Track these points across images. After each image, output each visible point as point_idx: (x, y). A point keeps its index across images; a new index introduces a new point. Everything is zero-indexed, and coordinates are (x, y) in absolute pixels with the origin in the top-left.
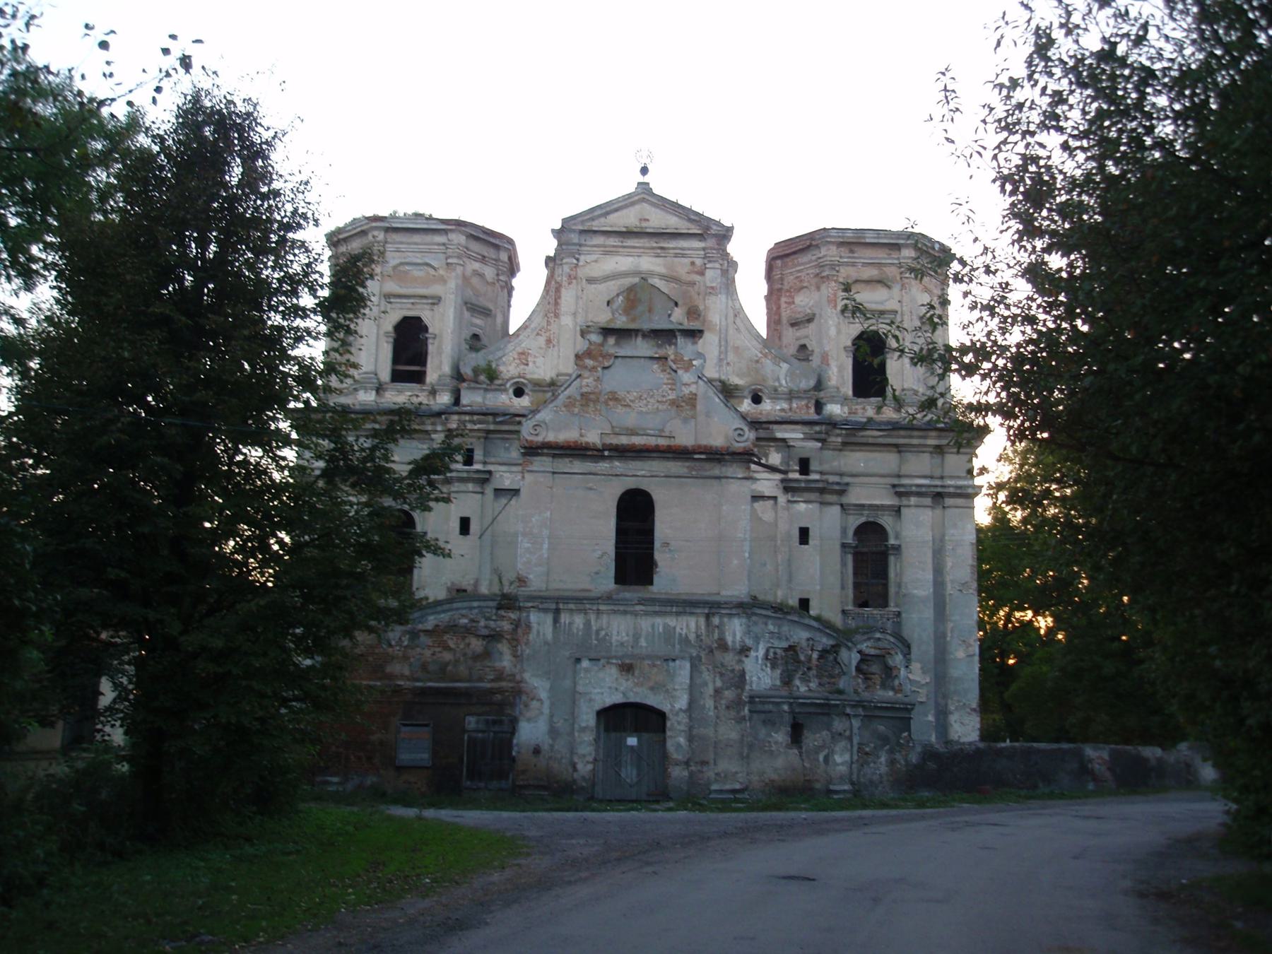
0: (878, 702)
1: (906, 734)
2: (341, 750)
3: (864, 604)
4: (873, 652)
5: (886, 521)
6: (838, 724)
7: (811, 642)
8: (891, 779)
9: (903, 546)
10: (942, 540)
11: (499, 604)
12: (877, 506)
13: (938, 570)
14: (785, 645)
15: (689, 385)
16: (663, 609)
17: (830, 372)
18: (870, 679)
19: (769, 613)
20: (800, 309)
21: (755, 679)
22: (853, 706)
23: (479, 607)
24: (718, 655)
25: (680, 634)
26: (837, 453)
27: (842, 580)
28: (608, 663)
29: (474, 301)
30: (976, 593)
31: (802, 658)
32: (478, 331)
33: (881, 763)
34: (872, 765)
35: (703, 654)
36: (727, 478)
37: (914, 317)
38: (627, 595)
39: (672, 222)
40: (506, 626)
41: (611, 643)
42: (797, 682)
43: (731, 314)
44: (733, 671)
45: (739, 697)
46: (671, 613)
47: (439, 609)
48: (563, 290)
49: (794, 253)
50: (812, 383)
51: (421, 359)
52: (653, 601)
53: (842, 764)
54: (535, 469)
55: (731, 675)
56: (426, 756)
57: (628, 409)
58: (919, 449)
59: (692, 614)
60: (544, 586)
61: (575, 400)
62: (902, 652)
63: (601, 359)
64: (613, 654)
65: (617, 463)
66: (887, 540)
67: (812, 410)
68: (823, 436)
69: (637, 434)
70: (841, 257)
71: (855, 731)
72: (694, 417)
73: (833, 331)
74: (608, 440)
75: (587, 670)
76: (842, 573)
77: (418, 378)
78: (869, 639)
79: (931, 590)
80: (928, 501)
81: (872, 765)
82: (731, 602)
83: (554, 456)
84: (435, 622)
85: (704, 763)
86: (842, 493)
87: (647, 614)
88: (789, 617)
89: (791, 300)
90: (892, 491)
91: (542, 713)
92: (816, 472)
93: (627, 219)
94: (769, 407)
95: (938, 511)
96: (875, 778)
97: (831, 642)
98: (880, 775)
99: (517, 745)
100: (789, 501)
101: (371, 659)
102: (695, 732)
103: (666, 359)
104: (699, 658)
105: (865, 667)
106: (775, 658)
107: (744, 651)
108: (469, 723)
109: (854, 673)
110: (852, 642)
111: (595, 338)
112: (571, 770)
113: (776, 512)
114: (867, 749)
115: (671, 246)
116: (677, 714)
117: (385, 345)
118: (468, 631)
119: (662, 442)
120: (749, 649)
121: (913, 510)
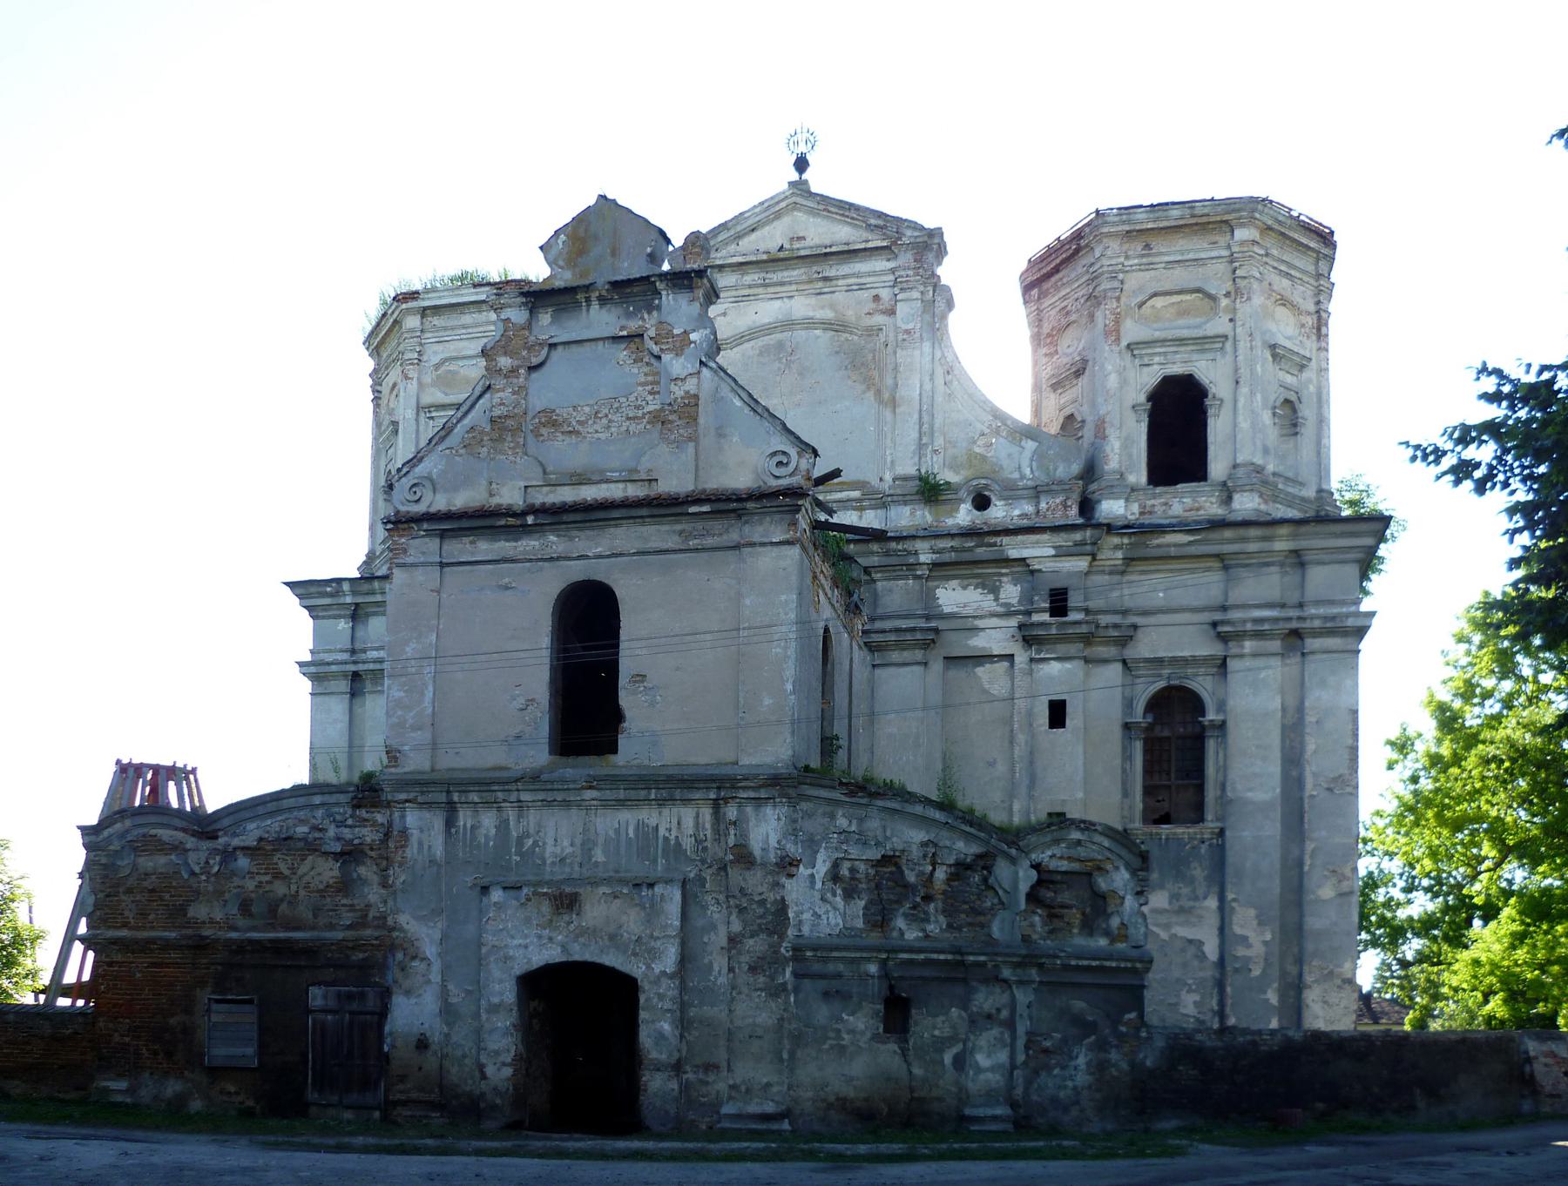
0: (1070, 956)
1: (1133, 1015)
2: (127, 1039)
3: (1165, 819)
4: (1064, 866)
5: (1203, 685)
6: (986, 999)
8: (1098, 1096)
9: (1230, 724)
10: (1300, 709)
14: (875, 854)
15: (683, 380)
16: (632, 794)
17: (1108, 449)
18: (1060, 917)
21: (806, 916)
22: (1016, 965)
23: (323, 804)
24: (736, 876)
25: (666, 839)
27: (1124, 783)
31: (911, 877)
34: (1056, 1071)
35: (707, 874)
36: (752, 545)
37: (1258, 343)
38: (569, 772)
39: (842, 234)
40: (369, 835)
42: (900, 923)
43: (939, 371)
44: (762, 903)
45: (775, 949)
50: (1076, 468)
52: (614, 781)
53: (992, 1069)
54: (409, 560)
55: (760, 911)
56: (250, 1051)
58: (1262, 562)
59: (686, 801)
60: (427, 766)
61: (482, 432)
62: (1128, 866)
63: (524, 353)
64: (547, 877)
66: (1203, 713)
70: (1127, 257)
71: (1021, 1008)
72: (693, 438)
73: (1113, 381)
76: (1124, 771)
78: (1057, 842)
79: (1278, 790)
80: (1275, 645)
82: (756, 776)
83: (443, 535)
84: (257, 833)
85: (710, 1067)
86: (1124, 641)
87: (605, 804)
90: (1212, 633)
91: (429, 982)
92: (1078, 609)
93: (771, 238)
94: (998, 512)
97: (974, 849)
98: (1075, 1088)
99: (391, 1034)
100: (1032, 660)
101: (167, 896)
102: (692, 1012)
103: (642, 335)
104: (701, 881)
105: (1050, 894)
106: (852, 879)
107: (787, 865)
109: (1023, 906)
110: (1019, 849)
111: (518, 315)
113: (1012, 679)
114: (1048, 1044)
115: (841, 273)
116: (657, 982)
118: (311, 847)
119: (634, 491)
120: (795, 863)
121: (1248, 663)
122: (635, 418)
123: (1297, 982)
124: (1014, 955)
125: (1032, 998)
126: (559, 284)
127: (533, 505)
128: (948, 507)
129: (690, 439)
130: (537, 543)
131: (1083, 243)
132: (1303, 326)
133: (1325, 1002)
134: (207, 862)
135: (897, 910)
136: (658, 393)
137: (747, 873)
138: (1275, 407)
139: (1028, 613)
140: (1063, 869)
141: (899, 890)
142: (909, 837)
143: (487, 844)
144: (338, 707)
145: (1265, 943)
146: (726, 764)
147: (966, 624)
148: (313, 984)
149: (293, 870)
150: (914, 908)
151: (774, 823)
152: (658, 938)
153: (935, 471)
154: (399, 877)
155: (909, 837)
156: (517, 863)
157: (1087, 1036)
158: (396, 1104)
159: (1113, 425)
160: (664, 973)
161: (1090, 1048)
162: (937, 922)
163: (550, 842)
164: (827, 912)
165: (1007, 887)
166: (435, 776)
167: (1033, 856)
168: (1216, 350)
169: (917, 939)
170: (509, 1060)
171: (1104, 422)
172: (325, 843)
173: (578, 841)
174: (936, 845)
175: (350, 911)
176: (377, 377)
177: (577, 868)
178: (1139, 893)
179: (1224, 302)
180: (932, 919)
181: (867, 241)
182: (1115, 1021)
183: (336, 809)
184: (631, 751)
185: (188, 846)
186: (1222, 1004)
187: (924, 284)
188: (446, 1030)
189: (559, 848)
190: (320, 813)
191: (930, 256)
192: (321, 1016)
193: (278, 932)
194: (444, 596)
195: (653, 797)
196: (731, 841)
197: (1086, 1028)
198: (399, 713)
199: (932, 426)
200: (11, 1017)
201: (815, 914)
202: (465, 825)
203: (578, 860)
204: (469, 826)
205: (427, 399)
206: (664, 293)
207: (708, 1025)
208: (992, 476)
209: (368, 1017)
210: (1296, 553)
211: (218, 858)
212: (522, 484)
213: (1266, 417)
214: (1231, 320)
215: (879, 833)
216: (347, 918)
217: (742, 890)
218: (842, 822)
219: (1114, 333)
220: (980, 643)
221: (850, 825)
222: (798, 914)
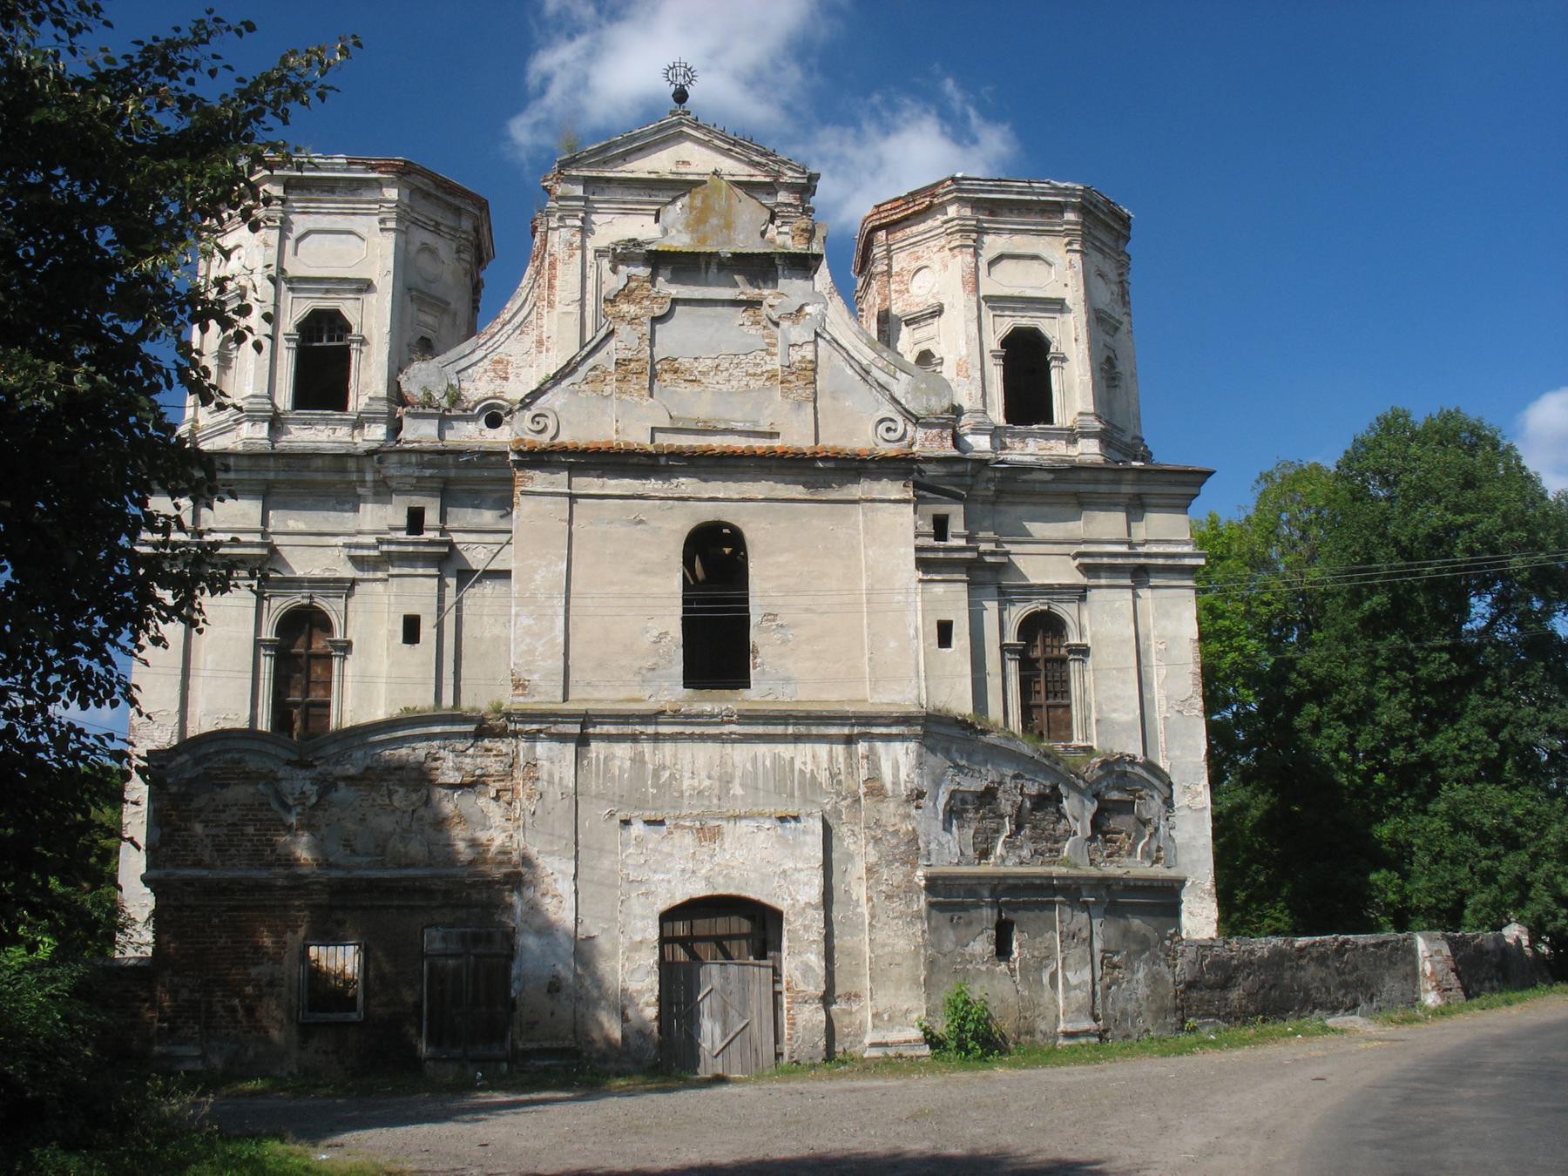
2: (197, 996)
5: (1066, 611)
20: (918, 300)
28: (677, 826)
30: (1201, 714)
32: (428, 334)
40: (493, 765)
48: (559, 266)
55: (894, 841)
57: (696, 388)
67: (949, 442)
68: (968, 481)
74: (665, 440)
75: (640, 841)
77: (337, 399)
89: (903, 287)
99: (518, 978)
114: (1116, 959)
122: (755, 375)
131: (936, 201)
137: (881, 806)
148: (429, 926)
152: (802, 870)
156: (653, 795)
157: (1143, 952)
160: (808, 904)
161: (1146, 963)
163: (687, 774)
172: (443, 774)
173: (716, 772)
177: (715, 801)
184: (760, 693)
189: (696, 781)
197: (1145, 944)
198: (528, 640)
204: (602, 757)
206: (780, 268)
207: (849, 954)
210: (1139, 496)
212: (650, 425)
222: (928, 843)
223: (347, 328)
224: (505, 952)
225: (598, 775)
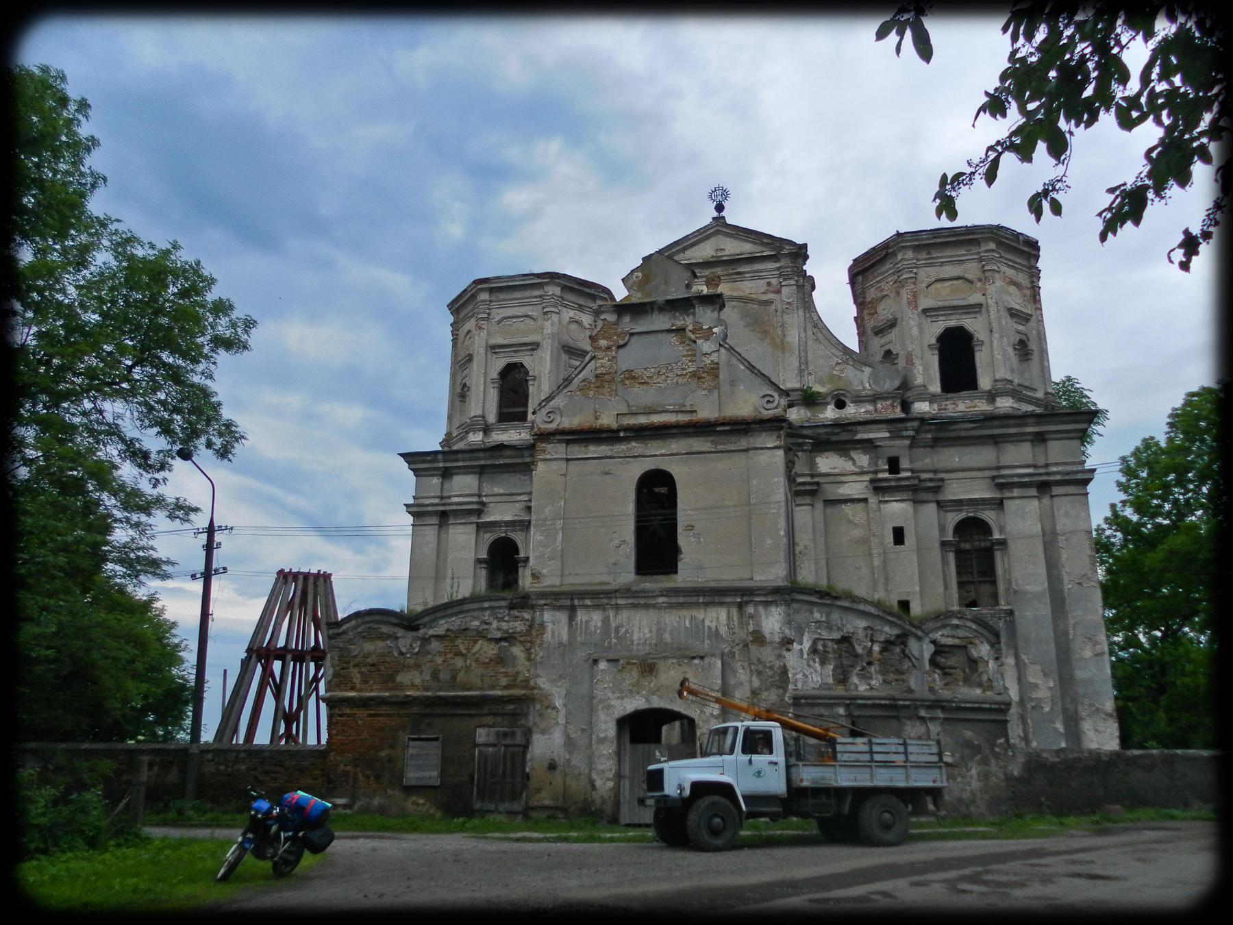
0: (960, 702)
1: (1002, 740)
2: (349, 768)
4: (950, 641)
5: (989, 516)
7: (870, 632)
8: (986, 797)
11: (511, 603)
12: (976, 500)
13: (1052, 565)
14: (837, 635)
16: (689, 600)
17: (916, 371)
18: (950, 674)
19: (813, 599)
20: (882, 318)
22: (929, 708)
25: (709, 628)
26: (929, 449)
28: (628, 663)
29: (571, 343)
31: (859, 650)
33: (971, 777)
34: (959, 779)
35: (736, 650)
36: (756, 449)
37: (1001, 308)
38: (648, 586)
39: (747, 248)
40: (519, 626)
41: (632, 642)
42: (855, 680)
46: (697, 604)
47: (450, 611)
49: (873, 266)
50: (897, 383)
51: (524, 399)
52: (677, 592)
54: (548, 457)
55: (770, 673)
56: (435, 774)
58: (1017, 439)
59: (721, 604)
62: (989, 642)
65: (634, 444)
66: (991, 534)
67: (898, 409)
69: (656, 412)
70: (918, 260)
72: (717, 387)
73: (915, 331)
76: (944, 572)
78: (944, 626)
79: (1046, 584)
81: (959, 779)
83: (568, 442)
84: (446, 626)
86: (937, 490)
87: (671, 606)
88: (839, 603)
91: (557, 724)
92: (907, 470)
93: (704, 251)
94: (852, 411)
95: (1046, 501)
96: (965, 795)
97: (896, 632)
98: (971, 791)
99: (531, 760)
101: (383, 668)
104: (732, 654)
105: (943, 660)
106: (825, 652)
107: (787, 643)
108: (480, 736)
110: (922, 631)
112: (589, 787)
117: (492, 390)
120: (790, 642)
123: (941, 721)
124: (927, 700)
125: (939, 729)
126: (634, 300)
127: (622, 425)
128: (824, 407)
129: (715, 388)
130: (625, 447)
131: (890, 251)
132: (1025, 296)
133: (1096, 730)
134: (411, 645)
135: (852, 671)
136: (694, 361)
137: (762, 649)
138: (1014, 345)
139: (876, 472)
140: (950, 643)
141: (852, 658)
142: (857, 625)
143: (595, 631)
144: (430, 533)
145: (1050, 689)
146: (745, 580)
147: (836, 478)
148: (479, 727)
149: (468, 650)
150: (862, 670)
151: (777, 617)
153: (811, 385)
154: (539, 653)
155: (857, 625)
158: (533, 809)
159: (917, 357)
162: (876, 679)
164: (811, 673)
165: (917, 656)
166: (564, 589)
167: (931, 635)
168: (976, 312)
169: (866, 690)
170: (611, 776)
171: (911, 355)
173: (654, 629)
174: (872, 629)
175: (505, 676)
176: (455, 327)
178: (997, 659)
179: (979, 284)
180: (874, 677)
181: (762, 252)
182: (993, 745)
183: (498, 611)
184: (685, 575)
185: (399, 635)
186: (1025, 731)
187: (798, 276)
188: (568, 757)
190: (487, 613)
191: (800, 261)
192: (484, 749)
193: (458, 691)
194: (568, 478)
195: (701, 600)
196: (751, 628)
197: (977, 749)
199: (806, 359)
200: (267, 754)
201: (804, 674)
202: (581, 620)
203: (654, 641)
205: (493, 341)
208: (845, 388)
209: (517, 748)
211: (419, 643)
212: (616, 413)
213: (1010, 351)
214: (984, 295)
215: (839, 622)
216: (504, 681)
217: (759, 660)
218: (817, 616)
219: (913, 303)
220: (846, 491)
221: (822, 617)
222: (795, 674)
223: (527, 373)
224: (523, 743)
225: (581, 631)
